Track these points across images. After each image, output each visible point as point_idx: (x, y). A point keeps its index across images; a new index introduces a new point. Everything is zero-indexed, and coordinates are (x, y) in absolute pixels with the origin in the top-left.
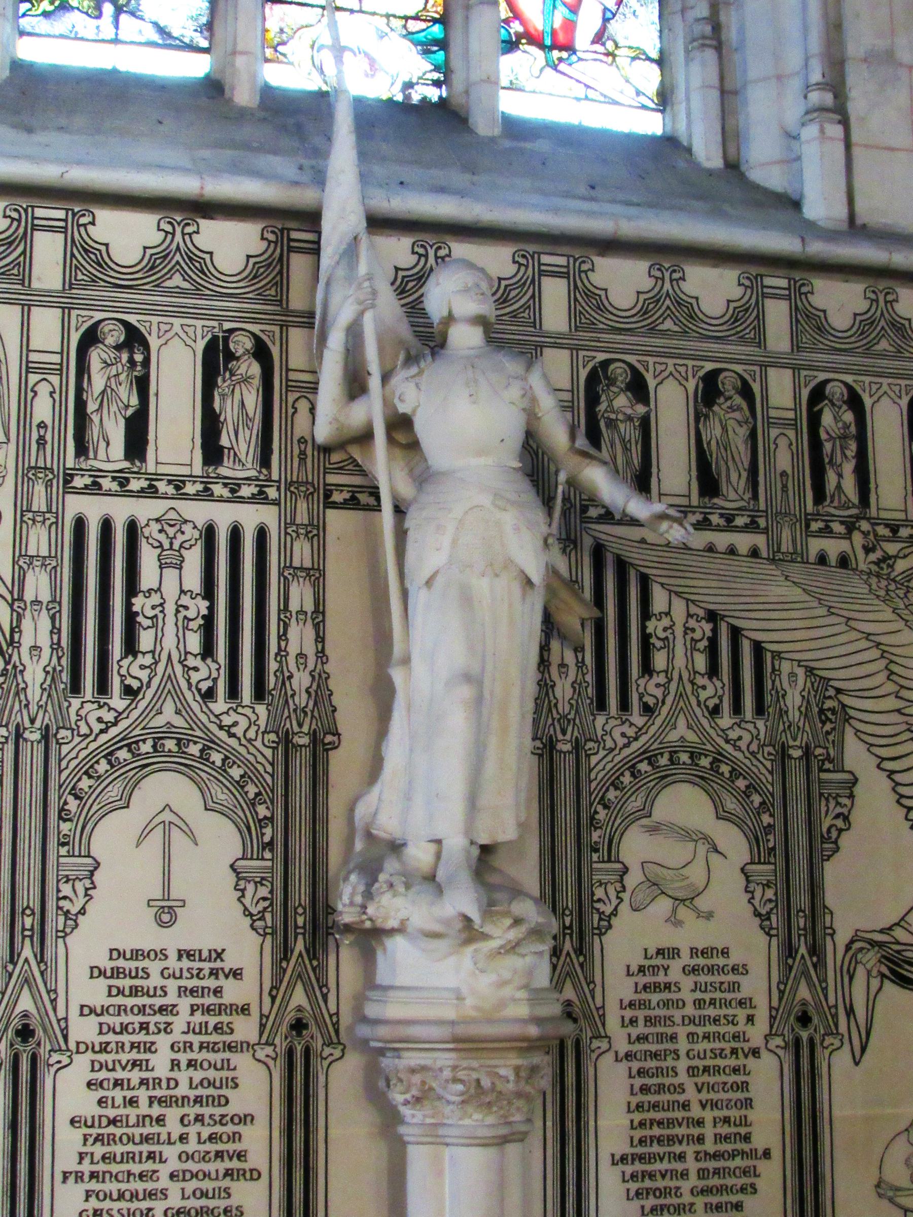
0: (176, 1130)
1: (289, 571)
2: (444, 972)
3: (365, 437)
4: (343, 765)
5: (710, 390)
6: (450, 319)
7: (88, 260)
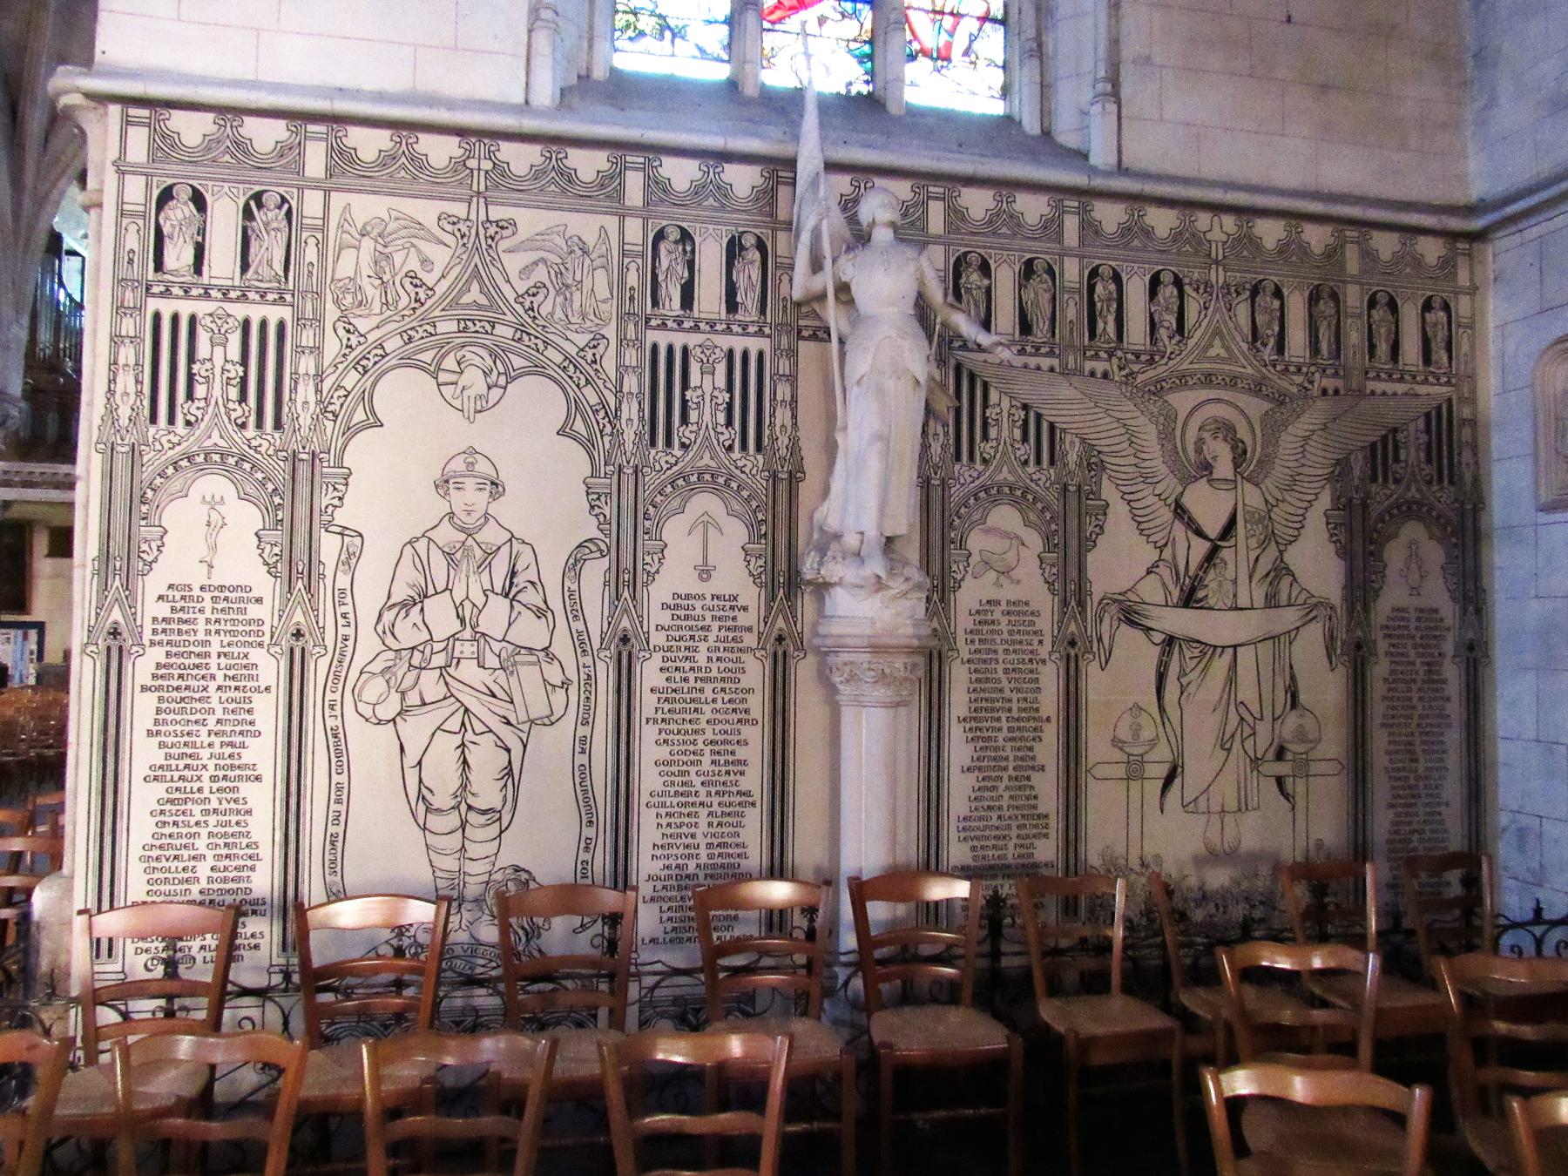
0: (710, 696)
1: (776, 375)
2: (865, 608)
3: (822, 297)
4: (806, 491)
5: (1028, 270)
6: (873, 223)
7: (657, 188)
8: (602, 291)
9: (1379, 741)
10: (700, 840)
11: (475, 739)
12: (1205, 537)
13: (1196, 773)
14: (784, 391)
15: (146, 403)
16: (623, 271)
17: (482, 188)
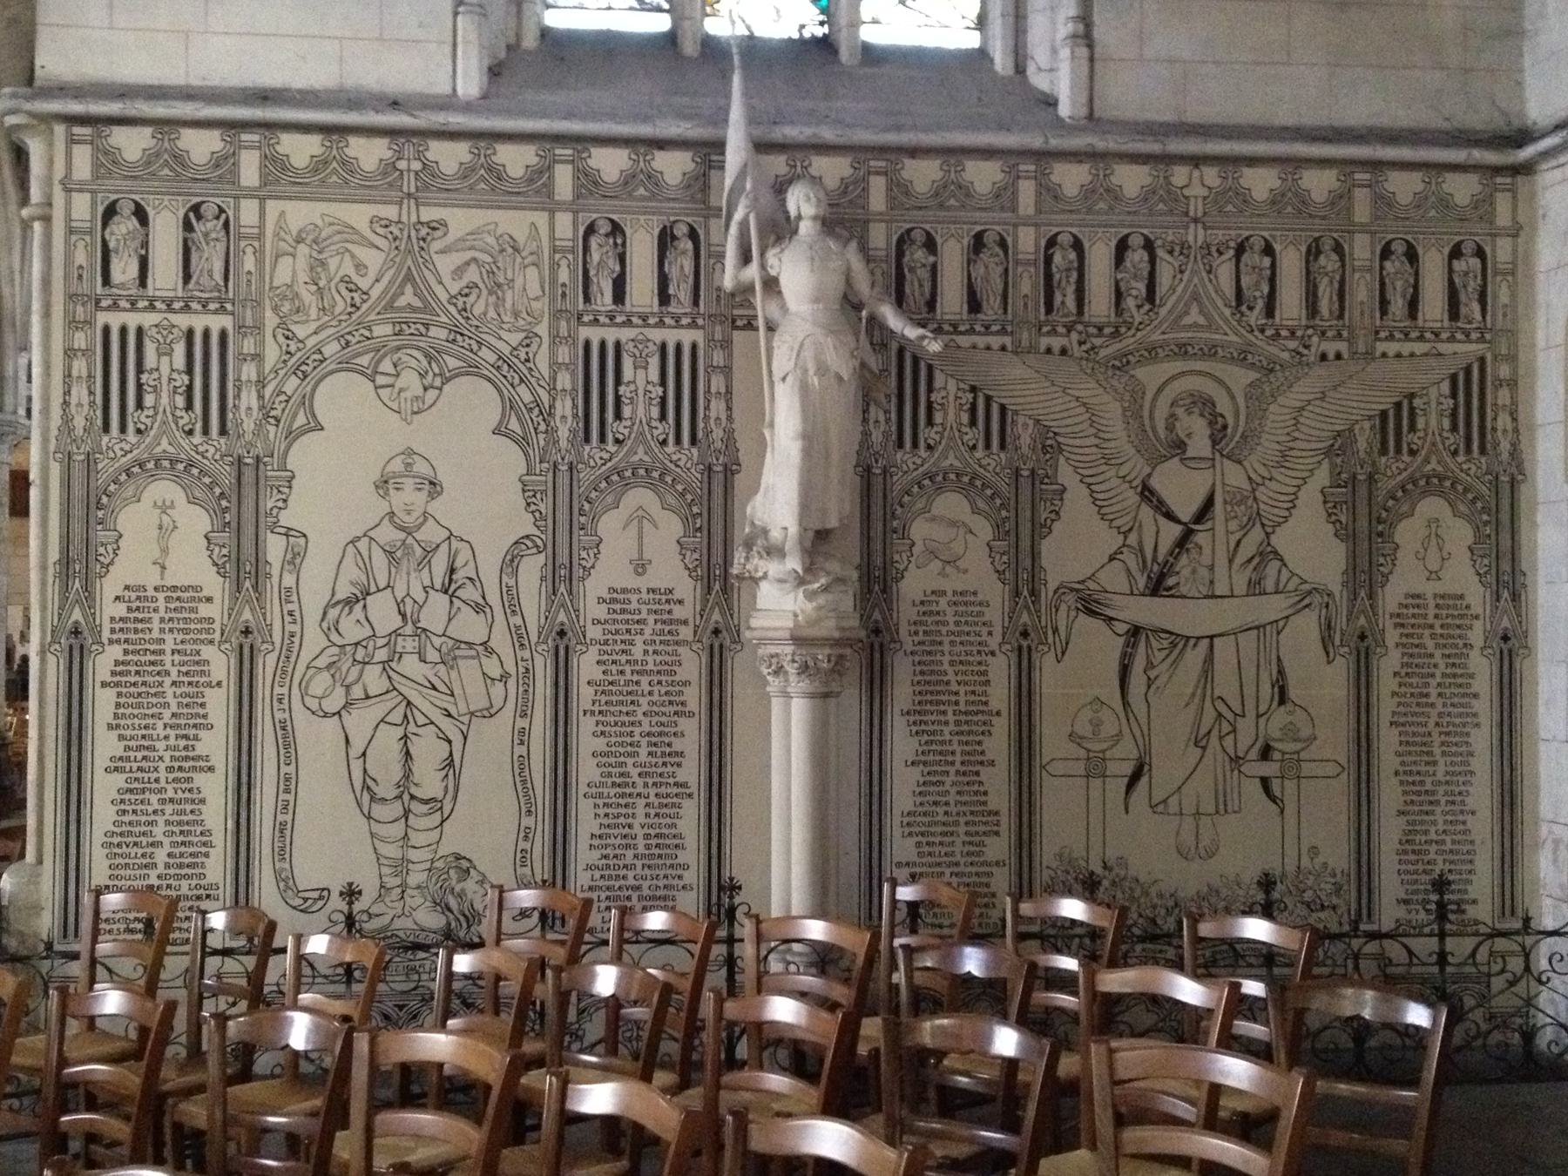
0: (647, 688)
4: (740, 481)
5: (978, 243)
7: (588, 182)
8: (534, 289)
9: (1388, 741)
10: (637, 829)
11: (415, 730)
12: (1178, 521)
13: (1164, 775)
14: (718, 383)
15: (99, 413)
16: (554, 266)
17: (413, 190)
